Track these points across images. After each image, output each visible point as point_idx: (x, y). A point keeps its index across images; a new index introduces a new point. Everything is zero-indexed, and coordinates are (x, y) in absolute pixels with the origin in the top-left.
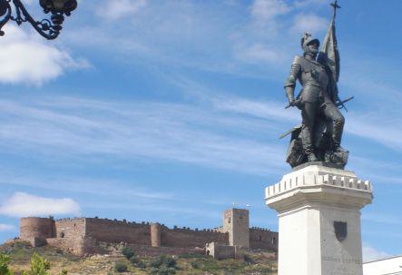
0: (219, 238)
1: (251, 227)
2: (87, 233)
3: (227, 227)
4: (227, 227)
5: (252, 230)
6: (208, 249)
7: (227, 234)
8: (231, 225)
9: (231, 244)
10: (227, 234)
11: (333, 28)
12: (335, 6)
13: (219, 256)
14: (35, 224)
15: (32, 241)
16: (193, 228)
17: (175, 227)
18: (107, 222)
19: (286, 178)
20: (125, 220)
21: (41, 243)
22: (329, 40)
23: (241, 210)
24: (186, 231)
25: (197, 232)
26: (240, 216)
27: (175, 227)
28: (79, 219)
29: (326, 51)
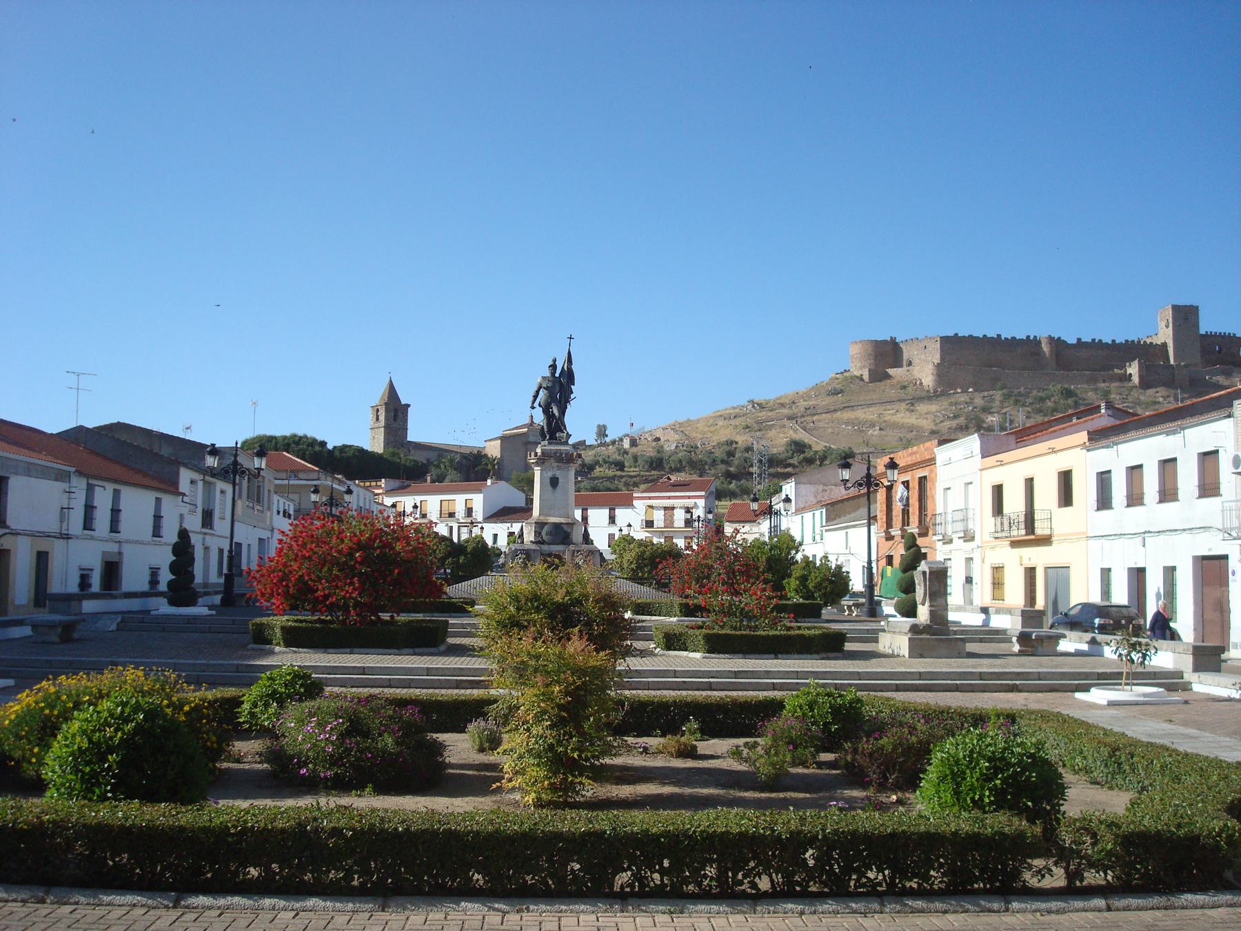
0: (1146, 352)
1: (1202, 332)
2: (942, 359)
3: (1164, 334)
4: (1164, 334)
5: (1207, 336)
6: (1129, 371)
7: (1164, 345)
9: (1172, 362)
10: (1164, 345)
11: (569, 353)
14: (870, 350)
15: (866, 377)
16: (1107, 340)
17: (1079, 340)
19: (49, 760)
20: (999, 336)
21: (879, 375)
24: (1096, 345)
25: (1114, 345)
26: (1185, 316)
27: (1079, 340)
29: (496, 439)
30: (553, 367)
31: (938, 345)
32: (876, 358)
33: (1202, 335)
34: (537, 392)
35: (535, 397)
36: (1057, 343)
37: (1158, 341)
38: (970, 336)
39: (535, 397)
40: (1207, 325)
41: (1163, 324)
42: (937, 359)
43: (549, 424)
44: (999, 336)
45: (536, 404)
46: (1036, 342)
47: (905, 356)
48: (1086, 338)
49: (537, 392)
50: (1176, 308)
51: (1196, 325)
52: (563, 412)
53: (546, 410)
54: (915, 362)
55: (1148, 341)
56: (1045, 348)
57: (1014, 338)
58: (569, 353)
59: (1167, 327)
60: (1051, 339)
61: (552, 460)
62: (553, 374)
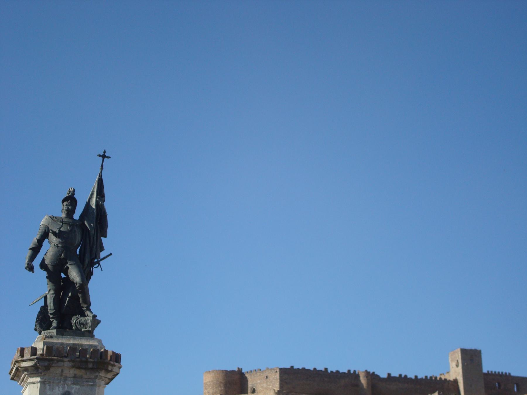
1: (485, 370)
2: (281, 386)
3: (455, 372)
4: (455, 372)
5: (489, 375)
7: (456, 381)
8: (460, 370)
10: (456, 381)
11: (100, 182)
12: (104, 156)
13: (76, 329)
14: (221, 379)
16: (411, 376)
17: (389, 375)
18: (304, 371)
20: (326, 369)
22: (92, 195)
23: (471, 350)
24: (403, 380)
26: (471, 358)
27: (389, 375)
28: (271, 369)
30: (71, 200)
31: (278, 376)
32: (226, 385)
33: (485, 374)
34: (40, 242)
35: (36, 250)
36: (372, 377)
37: (451, 377)
38: (304, 369)
39: (36, 250)
40: (488, 365)
41: (454, 364)
42: (277, 387)
43: (58, 301)
44: (326, 369)
45: (36, 263)
46: (355, 376)
47: (250, 384)
48: (395, 374)
49: (40, 242)
50: (464, 352)
51: (479, 365)
52: (87, 275)
53: (55, 272)
54: (259, 389)
55: (443, 378)
56: (363, 381)
57: (338, 372)
58: (100, 182)
59: (457, 366)
60: (367, 373)
61: (67, 364)
62: (70, 212)
